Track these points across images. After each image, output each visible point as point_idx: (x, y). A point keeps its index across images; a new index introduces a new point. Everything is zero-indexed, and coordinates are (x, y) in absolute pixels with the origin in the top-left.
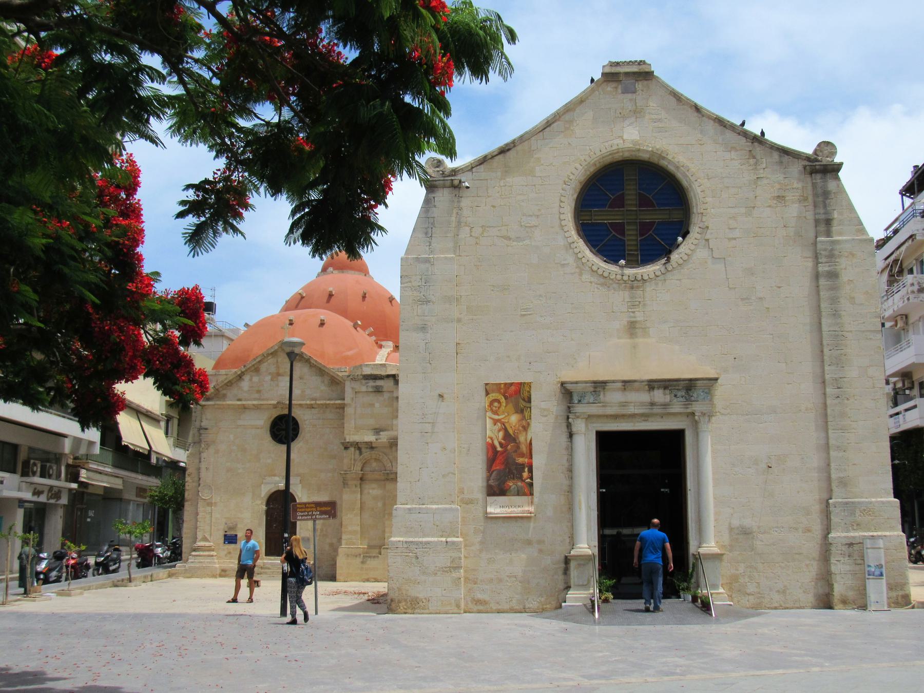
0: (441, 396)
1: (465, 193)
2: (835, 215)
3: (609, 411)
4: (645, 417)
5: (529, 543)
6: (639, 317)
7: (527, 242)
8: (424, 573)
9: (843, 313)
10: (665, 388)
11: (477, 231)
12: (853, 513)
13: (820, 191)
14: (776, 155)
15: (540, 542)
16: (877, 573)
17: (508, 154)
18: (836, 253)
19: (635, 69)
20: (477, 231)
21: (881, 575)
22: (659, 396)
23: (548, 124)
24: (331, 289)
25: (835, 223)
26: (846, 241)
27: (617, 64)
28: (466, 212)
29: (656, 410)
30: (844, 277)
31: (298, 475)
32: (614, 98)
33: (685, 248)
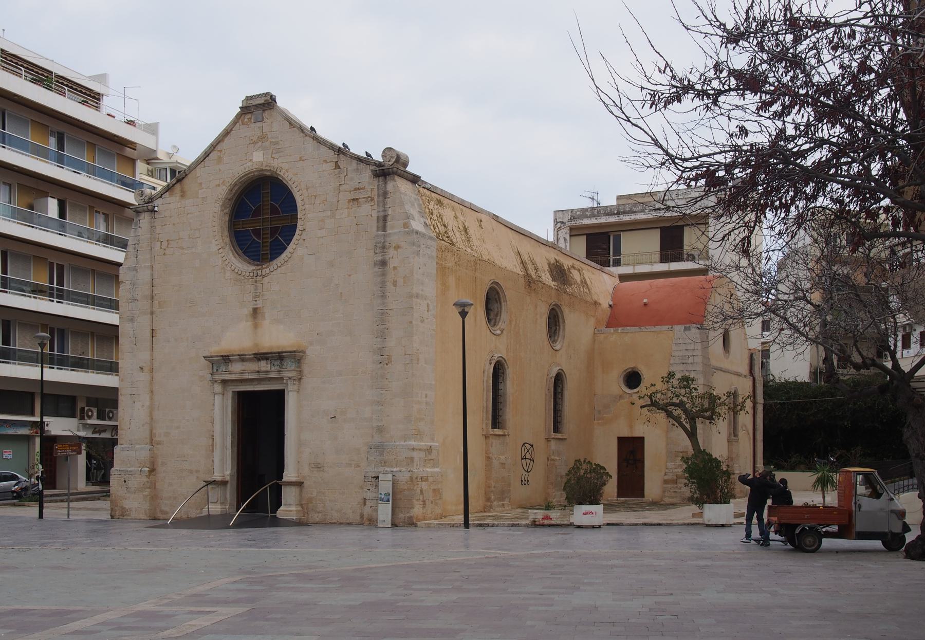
0: (141, 368)
1: (157, 215)
2: (390, 212)
3: (234, 377)
4: (259, 381)
5: (191, 472)
6: (259, 304)
7: (194, 250)
8: (129, 492)
9: (388, 294)
10: (267, 359)
11: (165, 244)
12: (382, 454)
13: (381, 192)
14: (354, 162)
15: (197, 471)
16: (386, 499)
17: (185, 180)
18: (387, 244)
19: (261, 101)
20: (165, 244)
21: (388, 501)
22: (264, 365)
23: (206, 154)
24: (645, 301)
25: (389, 218)
26: (395, 233)
27: (251, 97)
28: (158, 230)
29: (262, 376)
30: (392, 264)
31: (631, 427)
32: (251, 130)
33: (296, 249)
